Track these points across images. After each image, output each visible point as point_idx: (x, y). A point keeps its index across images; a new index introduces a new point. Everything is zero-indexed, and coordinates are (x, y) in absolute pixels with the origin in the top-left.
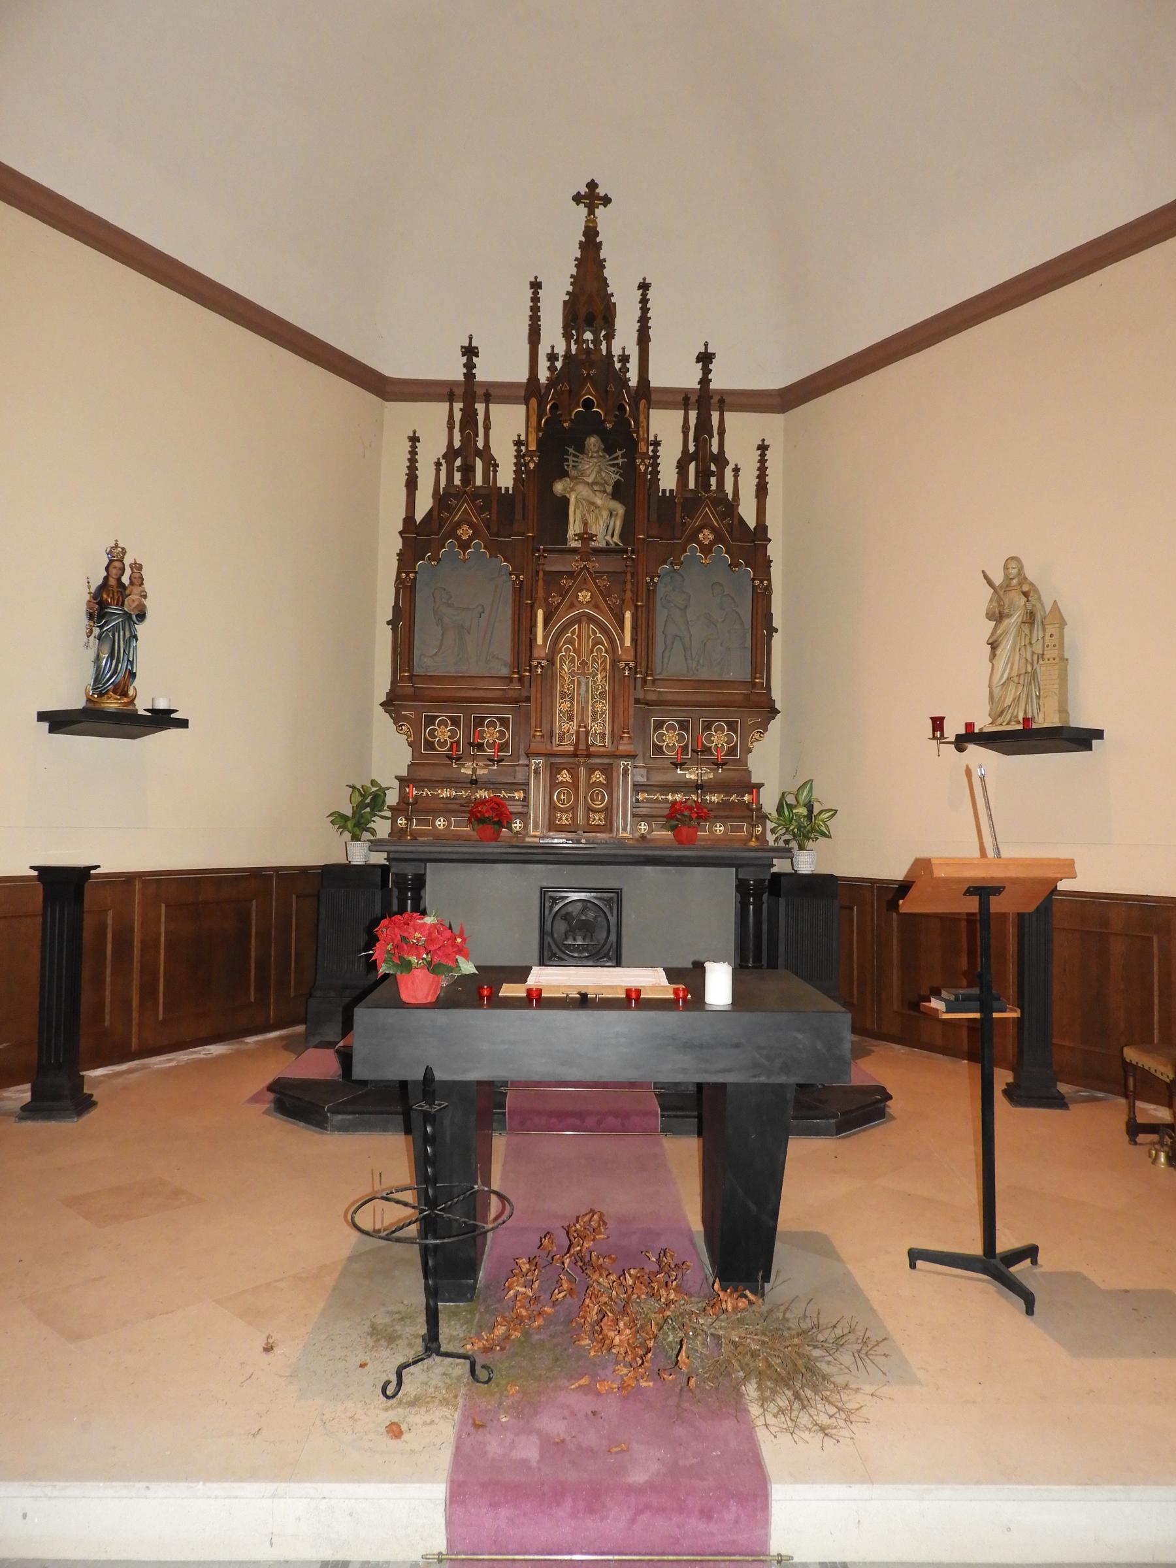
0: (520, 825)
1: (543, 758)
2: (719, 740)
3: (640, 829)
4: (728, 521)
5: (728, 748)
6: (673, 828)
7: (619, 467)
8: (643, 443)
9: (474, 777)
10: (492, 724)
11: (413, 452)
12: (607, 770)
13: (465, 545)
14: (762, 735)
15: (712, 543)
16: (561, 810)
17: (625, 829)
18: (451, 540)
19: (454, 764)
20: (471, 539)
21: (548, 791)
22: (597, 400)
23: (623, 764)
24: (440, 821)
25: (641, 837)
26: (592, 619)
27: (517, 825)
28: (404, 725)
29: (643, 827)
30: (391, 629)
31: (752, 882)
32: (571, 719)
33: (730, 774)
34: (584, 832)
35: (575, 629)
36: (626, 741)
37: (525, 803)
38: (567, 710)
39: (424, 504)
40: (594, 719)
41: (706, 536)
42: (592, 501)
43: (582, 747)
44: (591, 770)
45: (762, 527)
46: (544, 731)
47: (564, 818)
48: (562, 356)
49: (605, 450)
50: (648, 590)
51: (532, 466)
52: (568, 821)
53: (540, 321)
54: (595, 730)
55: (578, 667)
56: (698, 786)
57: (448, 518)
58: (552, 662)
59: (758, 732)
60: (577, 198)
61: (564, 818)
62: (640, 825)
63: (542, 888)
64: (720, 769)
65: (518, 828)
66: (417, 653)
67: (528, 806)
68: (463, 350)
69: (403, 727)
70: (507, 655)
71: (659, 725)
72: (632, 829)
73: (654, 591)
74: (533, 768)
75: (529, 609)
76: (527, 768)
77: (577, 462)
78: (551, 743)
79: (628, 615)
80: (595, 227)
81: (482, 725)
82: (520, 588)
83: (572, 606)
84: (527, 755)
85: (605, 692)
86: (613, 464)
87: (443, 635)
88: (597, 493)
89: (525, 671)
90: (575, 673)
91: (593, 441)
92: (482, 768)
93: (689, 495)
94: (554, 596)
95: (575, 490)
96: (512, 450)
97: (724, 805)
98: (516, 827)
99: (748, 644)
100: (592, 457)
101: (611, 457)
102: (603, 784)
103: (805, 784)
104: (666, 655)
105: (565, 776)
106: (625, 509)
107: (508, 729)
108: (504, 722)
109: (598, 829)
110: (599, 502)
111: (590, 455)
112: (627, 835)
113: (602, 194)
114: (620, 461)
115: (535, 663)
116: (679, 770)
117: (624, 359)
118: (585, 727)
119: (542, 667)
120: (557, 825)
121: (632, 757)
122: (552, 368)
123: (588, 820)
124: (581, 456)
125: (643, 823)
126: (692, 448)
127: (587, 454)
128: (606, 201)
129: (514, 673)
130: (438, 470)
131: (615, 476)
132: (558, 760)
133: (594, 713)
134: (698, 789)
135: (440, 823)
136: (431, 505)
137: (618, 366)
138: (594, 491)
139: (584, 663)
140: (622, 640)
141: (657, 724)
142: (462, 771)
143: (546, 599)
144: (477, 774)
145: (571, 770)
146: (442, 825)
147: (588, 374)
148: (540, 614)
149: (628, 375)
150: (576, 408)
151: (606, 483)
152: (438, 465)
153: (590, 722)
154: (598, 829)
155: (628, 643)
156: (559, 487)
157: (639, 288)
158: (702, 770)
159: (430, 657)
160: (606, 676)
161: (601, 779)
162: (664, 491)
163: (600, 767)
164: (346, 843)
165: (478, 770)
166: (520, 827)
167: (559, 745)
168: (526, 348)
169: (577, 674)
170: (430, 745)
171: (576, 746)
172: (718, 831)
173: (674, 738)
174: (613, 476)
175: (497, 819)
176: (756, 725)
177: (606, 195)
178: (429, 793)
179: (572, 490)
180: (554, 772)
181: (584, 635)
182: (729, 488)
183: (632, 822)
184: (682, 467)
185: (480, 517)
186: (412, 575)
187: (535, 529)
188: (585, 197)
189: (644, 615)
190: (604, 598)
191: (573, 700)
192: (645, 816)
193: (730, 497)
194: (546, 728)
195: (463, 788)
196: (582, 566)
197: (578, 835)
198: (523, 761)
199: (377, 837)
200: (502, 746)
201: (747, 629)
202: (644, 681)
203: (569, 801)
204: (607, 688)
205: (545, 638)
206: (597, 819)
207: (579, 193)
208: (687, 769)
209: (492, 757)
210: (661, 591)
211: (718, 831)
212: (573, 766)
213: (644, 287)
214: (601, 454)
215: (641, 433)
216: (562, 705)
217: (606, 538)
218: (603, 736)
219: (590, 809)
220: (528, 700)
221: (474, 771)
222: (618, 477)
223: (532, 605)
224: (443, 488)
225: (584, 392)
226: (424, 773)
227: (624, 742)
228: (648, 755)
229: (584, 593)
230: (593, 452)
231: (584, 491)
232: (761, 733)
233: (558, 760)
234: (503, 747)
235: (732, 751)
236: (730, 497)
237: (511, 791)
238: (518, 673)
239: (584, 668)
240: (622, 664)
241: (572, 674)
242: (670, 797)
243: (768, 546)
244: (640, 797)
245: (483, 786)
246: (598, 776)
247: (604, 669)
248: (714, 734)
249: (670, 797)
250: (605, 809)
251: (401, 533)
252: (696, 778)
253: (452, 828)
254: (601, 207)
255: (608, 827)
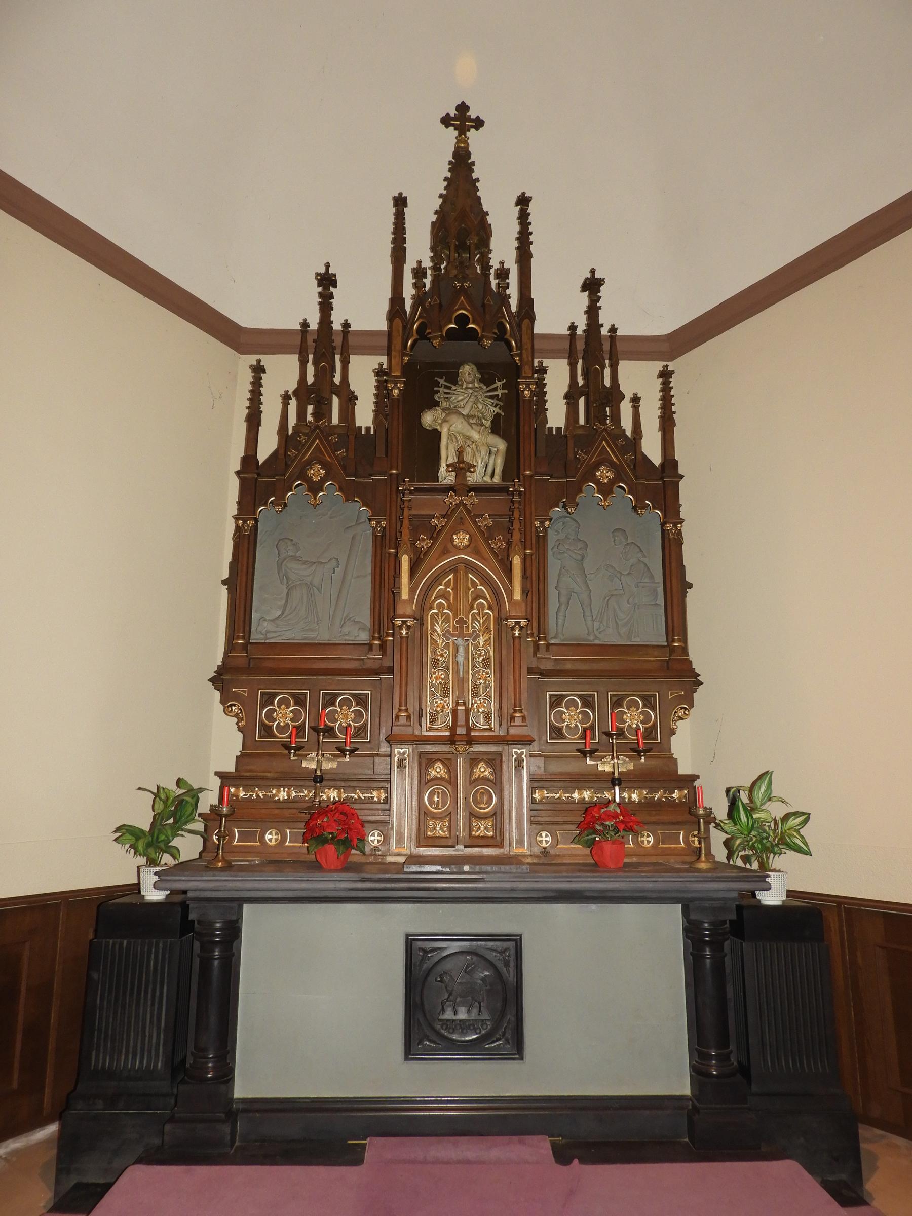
0: (379, 838)
1: (410, 747)
2: (633, 718)
3: (541, 841)
4: (630, 456)
5: (646, 729)
6: (591, 844)
7: (498, 399)
8: (527, 367)
9: (319, 773)
10: (346, 703)
11: (257, 384)
12: (494, 761)
13: (315, 488)
14: (687, 713)
15: (612, 482)
16: (435, 817)
17: (520, 842)
18: (299, 482)
19: (292, 756)
20: (324, 480)
21: (415, 790)
22: (472, 315)
23: (516, 753)
24: (271, 834)
25: (542, 853)
26: (470, 567)
27: (374, 838)
28: (234, 705)
29: (545, 839)
30: (227, 589)
31: (706, 925)
32: (446, 694)
33: (653, 762)
34: (465, 847)
35: (450, 579)
36: (518, 721)
37: (387, 806)
38: (440, 683)
39: (267, 445)
40: (475, 694)
41: (604, 474)
42: (468, 434)
43: (461, 731)
44: (473, 762)
45: (670, 464)
46: (411, 710)
47: (438, 828)
48: (429, 268)
49: (481, 381)
50: (538, 536)
51: (396, 392)
52: (445, 832)
53: (405, 243)
54: (478, 707)
55: (454, 626)
56: (614, 781)
57: (296, 456)
58: (420, 619)
59: (682, 708)
60: (446, 121)
61: (438, 828)
62: (541, 836)
63: (407, 935)
64: (643, 758)
65: (376, 842)
66: (255, 616)
67: (390, 810)
68: (319, 278)
69: (234, 708)
70: (365, 616)
71: (557, 702)
72: (530, 843)
73: (545, 537)
74: (396, 759)
75: (392, 559)
76: (388, 759)
77: (449, 393)
78: (421, 726)
79: (517, 561)
80: (467, 148)
81: (333, 704)
82: (382, 536)
83: (445, 552)
84: (388, 740)
85: (489, 658)
86: (491, 395)
87: (287, 594)
88: (473, 426)
89: (388, 635)
90: (450, 634)
91: (467, 371)
92: (329, 759)
93: (580, 432)
94: (423, 540)
95: (447, 421)
96: (372, 381)
97: (648, 805)
98: (373, 841)
99: (661, 601)
100: (466, 388)
101: (489, 388)
102: (489, 780)
103: (761, 777)
104: (561, 614)
105: (438, 770)
106: (506, 445)
107: (366, 709)
108: (361, 700)
109: (484, 842)
110: (476, 436)
111: (464, 386)
112: (525, 850)
113: (473, 116)
114: (499, 392)
115: (398, 622)
116: (588, 759)
117: (503, 274)
118: (464, 704)
119: (408, 628)
120: (428, 837)
121: (526, 741)
122: (419, 286)
123: (471, 830)
124: (454, 387)
125: (544, 834)
126: (581, 381)
127: (462, 385)
128: (479, 123)
129: (374, 638)
130: (286, 404)
131: (494, 409)
132: (429, 748)
133: (476, 687)
134: (614, 785)
135: (271, 837)
136: (276, 447)
137: (494, 282)
138: (470, 424)
139: (462, 622)
140: (510, 594)
141: (554, 699)
142: (303, 765)
143: (413, 544)
144: (323, 768)
145: (446, 761)
146: (273, 840)
147: (462, 286)
148: (405, 561)
149: (508, 292)
150: (448, 325)
151: (484, 417)
152: (286, 398)
153: (470, 697)
154: (484, 842)
155: (517, 596)
156: (428, 419)
157: (517, 204)
158: (619, 759)
159: (271, 621)
160: (490, 638)
161: (487, 773)
162: (551, 429)
163: (485, 757)
164: (139, 868)
165: (324, 763)
166: (379, 841)
167: (430, 729)
168: (388, 268)
169: (453, 635)
170: (267, 730)
171: (453, 729)
172: (646, 842)
173: (575, 717)
174: (492, 409)
175: (343, 837)
176: (681, 700)
177: (478, 117)
178: (261, 795)
179: (444, 421)
180: (423, 765)
181: (461, 588)
182: (626, 423)
183: (529, 830)
184: (571, 397)
185: (335, 455)
186: (250, 523)
187: (400, 464)
188: (455, 118)
189: (534, 568)
190: (486, 540)
191: (448, 669)
192: (547, 823)
193: (629, 433)
194: (413, 706)
195: (306, 787)
196: (458, 502)
197: (457, 850)
198: (384, 749)
199: (181, 860)
200: (358, 731)
201: (658, 583)
202: (537, 648)
203: (444, 804)
204: (492, 653)
205: (412, 591)
206: (482, 828)
207: (448, 115)
208: (601, 758)
209: (343, 745)
210: (552, 537)
211: (646, 842)
212: (449, 756)
213: (523, 201)
214: (477, 385)
215: (524, 356)
216: (434, 676)
217: (484, 478)
218: (487, 717)
219: (473, 815)
220: (390, 671)
221: (319, 765)
222: (497, 410)
223: (396, 554)
224: (293, 427)
225: (456, 307)
226: (257, 766)
227: (516, 723)
228: (544, 738)
229: (461, 535)
230: (468, 383)
231: (458, 424)
232: (685, 709)
233: (429, 748)
234: (361, 731)
235: (650, 732)
236: (629, 433)
237: (369, 789)
238: (379, 639)
239: (461, 628)
240: (511, 622)
241: (445, 635)
242: (576, 795)
243: (680, 483)
244: (537, 796)
245: (331, 783)
246: (483, 770)
247: (488, 630)
248: (626, 711)
249: (576, 795)
250: (494, 814)
251: (238, 473)
252: (612, 770)
253: (287, 844)
254: (472, 130)
255: (496, 841)
